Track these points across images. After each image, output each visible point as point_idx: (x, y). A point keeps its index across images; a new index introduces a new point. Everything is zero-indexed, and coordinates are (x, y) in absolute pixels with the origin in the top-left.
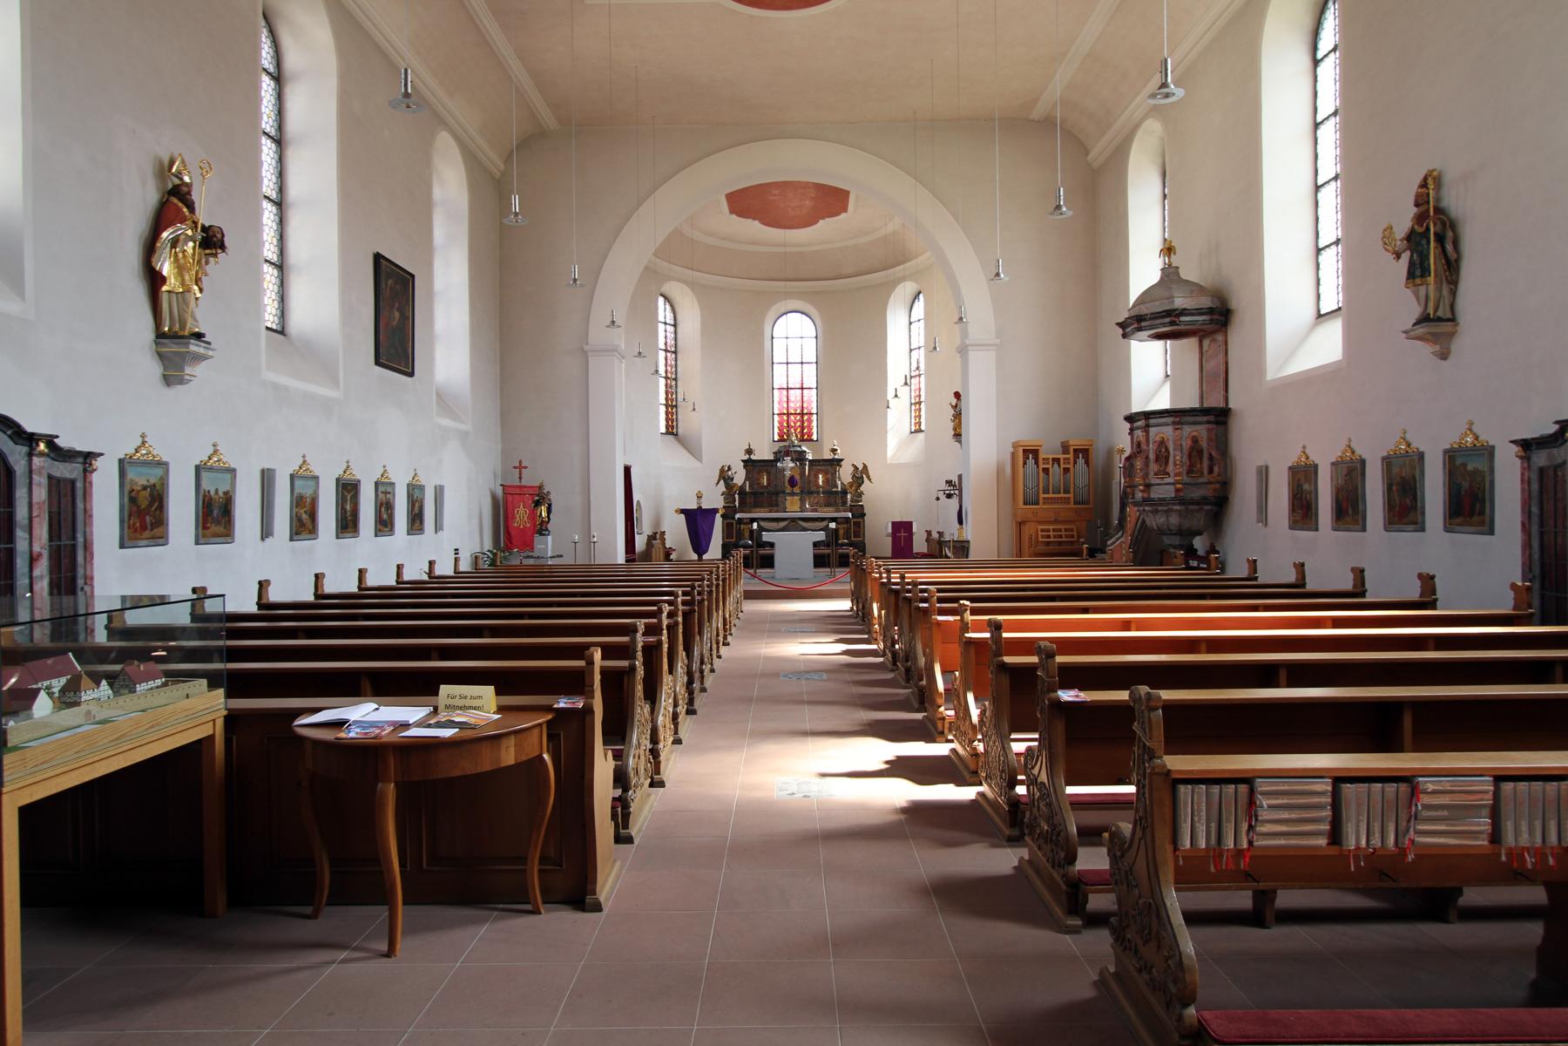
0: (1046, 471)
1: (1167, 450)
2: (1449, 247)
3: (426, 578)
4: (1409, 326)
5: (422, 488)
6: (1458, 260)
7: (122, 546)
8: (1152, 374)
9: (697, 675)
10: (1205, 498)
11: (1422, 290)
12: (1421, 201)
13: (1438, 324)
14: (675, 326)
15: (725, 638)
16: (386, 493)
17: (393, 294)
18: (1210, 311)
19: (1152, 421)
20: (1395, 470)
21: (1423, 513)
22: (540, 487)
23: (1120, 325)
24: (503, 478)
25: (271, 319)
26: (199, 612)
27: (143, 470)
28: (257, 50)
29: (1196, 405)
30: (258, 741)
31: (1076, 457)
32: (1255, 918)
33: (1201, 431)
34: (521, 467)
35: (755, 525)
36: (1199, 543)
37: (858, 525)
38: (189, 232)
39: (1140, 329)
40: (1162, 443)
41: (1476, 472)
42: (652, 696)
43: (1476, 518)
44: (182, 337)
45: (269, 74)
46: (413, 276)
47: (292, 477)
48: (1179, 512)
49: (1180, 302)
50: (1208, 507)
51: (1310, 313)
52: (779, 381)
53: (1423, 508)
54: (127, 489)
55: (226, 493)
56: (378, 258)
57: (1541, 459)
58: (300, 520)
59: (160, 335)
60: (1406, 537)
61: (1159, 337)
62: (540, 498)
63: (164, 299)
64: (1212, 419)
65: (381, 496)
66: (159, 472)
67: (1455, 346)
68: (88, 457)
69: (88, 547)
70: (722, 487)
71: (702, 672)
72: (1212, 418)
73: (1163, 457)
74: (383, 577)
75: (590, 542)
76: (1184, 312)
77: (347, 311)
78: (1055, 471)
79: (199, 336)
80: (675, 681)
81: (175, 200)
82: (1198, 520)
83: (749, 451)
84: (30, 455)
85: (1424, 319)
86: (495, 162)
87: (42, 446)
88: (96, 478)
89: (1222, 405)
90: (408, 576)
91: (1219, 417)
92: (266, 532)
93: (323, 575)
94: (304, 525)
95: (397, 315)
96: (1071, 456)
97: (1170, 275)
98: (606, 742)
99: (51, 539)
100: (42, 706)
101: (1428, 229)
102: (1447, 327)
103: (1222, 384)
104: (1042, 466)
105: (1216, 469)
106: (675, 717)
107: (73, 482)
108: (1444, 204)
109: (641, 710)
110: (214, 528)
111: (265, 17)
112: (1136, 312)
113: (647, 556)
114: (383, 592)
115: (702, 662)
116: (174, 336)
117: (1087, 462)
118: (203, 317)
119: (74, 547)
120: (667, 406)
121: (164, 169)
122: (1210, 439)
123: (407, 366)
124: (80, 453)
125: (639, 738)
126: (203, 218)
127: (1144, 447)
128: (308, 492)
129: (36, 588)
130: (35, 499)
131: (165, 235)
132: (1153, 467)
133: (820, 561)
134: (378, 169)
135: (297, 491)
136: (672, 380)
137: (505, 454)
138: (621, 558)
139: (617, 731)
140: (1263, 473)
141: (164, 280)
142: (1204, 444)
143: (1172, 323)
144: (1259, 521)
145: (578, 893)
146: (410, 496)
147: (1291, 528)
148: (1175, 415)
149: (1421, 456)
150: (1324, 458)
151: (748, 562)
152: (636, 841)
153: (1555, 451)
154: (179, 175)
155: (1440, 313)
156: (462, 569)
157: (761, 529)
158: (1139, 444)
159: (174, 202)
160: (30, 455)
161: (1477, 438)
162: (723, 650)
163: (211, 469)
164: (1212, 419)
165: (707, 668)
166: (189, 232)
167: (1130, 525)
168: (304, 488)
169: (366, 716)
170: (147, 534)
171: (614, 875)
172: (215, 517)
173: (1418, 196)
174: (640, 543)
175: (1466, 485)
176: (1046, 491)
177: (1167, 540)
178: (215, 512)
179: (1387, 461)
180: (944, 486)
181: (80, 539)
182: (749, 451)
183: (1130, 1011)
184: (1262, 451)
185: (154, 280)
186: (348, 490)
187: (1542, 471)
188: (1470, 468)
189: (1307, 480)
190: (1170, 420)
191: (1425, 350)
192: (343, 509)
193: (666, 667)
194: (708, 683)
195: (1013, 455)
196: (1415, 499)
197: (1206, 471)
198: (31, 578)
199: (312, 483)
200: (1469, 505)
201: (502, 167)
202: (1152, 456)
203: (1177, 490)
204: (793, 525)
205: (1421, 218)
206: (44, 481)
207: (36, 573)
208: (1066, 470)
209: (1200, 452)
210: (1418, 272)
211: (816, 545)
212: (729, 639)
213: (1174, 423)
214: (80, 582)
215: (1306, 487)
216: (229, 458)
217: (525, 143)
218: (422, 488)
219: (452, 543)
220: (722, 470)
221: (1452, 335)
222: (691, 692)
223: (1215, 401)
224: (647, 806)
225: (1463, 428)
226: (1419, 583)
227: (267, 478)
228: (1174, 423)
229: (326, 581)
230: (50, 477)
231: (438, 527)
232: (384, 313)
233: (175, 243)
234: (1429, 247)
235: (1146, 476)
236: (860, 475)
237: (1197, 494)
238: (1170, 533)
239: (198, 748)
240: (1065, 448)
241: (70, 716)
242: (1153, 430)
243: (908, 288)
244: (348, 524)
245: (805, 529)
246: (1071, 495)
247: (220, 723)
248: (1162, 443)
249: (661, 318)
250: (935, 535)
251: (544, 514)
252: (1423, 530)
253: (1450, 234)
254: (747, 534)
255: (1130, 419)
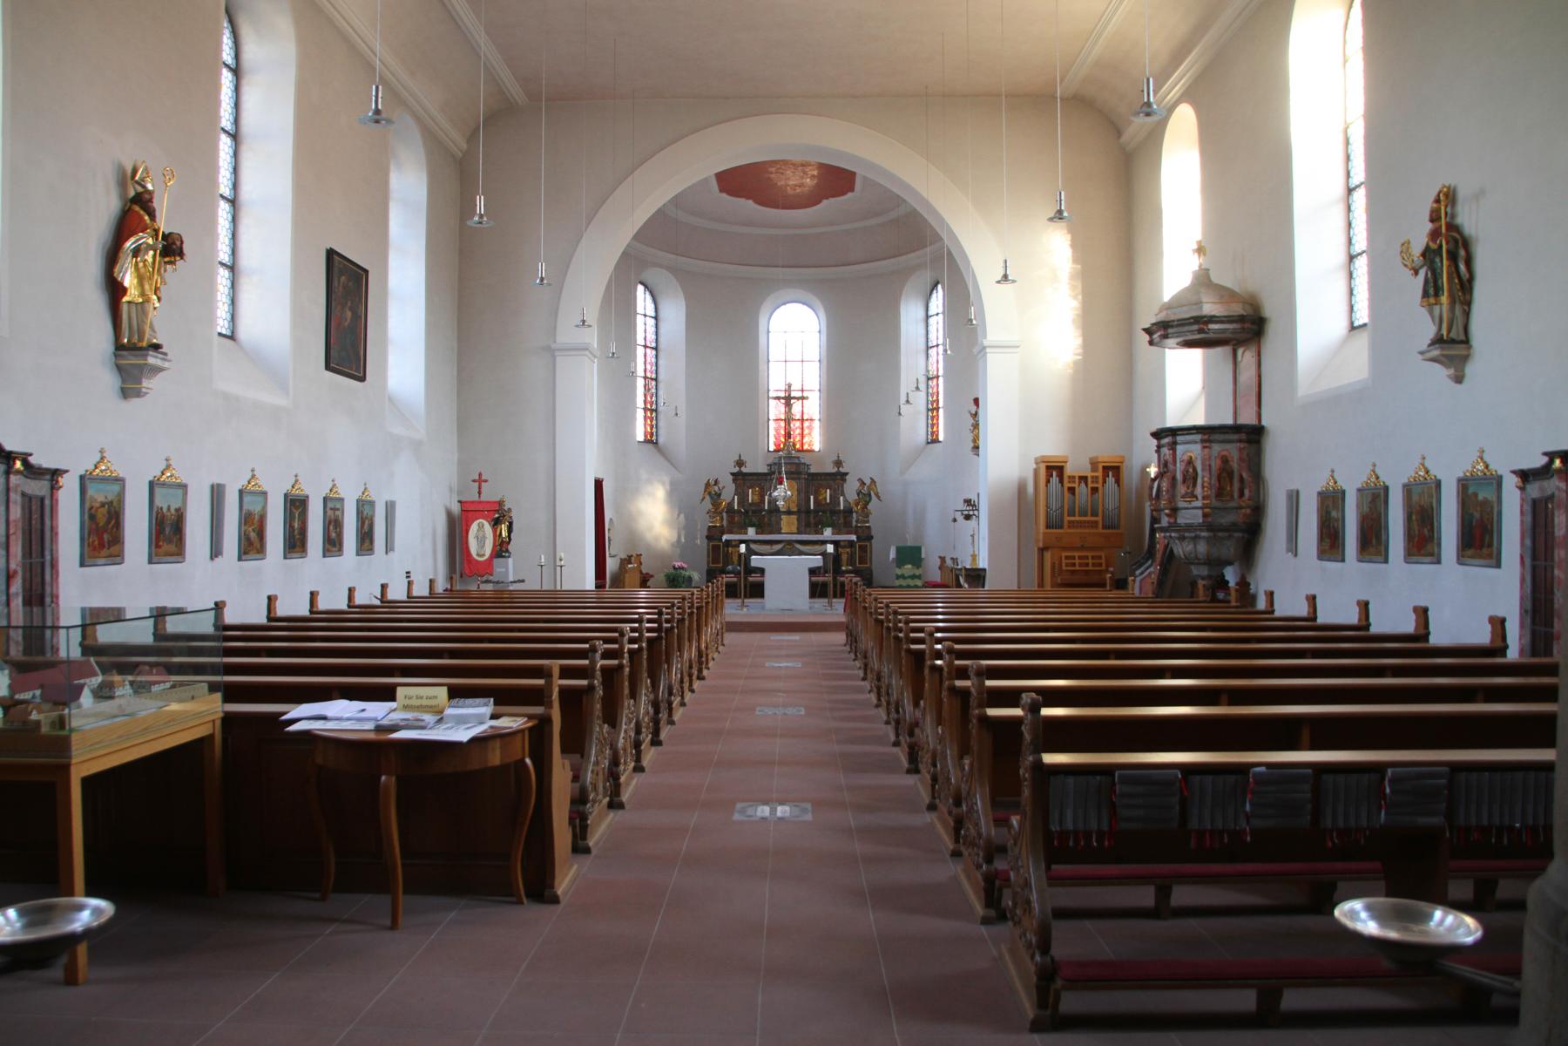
0: (1072, 490)
1: (1195, 470)
2: (1462, 267)
3: (378, 603)
4: (1424, 347)
5: (372, 504)
6: (1471, 279)
7: (82, 565)
8: (1186, 385)
9: (663, 706)
10: (1234, 524)
11: (1437, 309)
12: (1435, 217)
13: (1453, 347)
14: (656, 318)
15: (700, 671)
16: (334, 509)
17: (346, 289)
18: (1241, 319)
19: (1179, 438)
20: (1415, 498)
21: (1439, 545)
22: (501, 503)
23: (1147, 331)
24: (459, 493)
25: (223, 326)
26: (89, 642)
27: (101, 486)
28: (219, 50)
29: (1230, 421)
30: (252, 744)
31: (1105, 476)
32: (1160, 911)
33: (1233, 451)
34: (480, 481)
35: (743, 548)
36: (1231, 575)
37: (863, 549)
38: (150, 241)
39: (1166, 337)
40: (1190, 462)
41: (1486, 502)
42: (611, 719)
43: (1485, 551)
44: (141, 349)
45: (227, 66)
46: (366, 272)
47: (241, 492)
48: (1208, 539)
49: (1209, 309)
50: (1237, 535)
51: (1341, 326)
52: (776, 385)
53: (1439, 538)
54: (87, 505)
55: (177, 510)
56: (331, 254)
57: (1534, 490)
58: (248, 539)
59: (119, 347)
60: (1424, 569)
61: (1190, 344)
62: (499, 515)
63: (125, 308)
64: (1241, 442)
65: (330, 513)
66: (116, 488)
67: (1470, 369)
68: (55, 474)
69: (54, 565)
70: (708, 504)
71: (670, 704)
72: (1243, 436)
73: (1191, 478)
74: (332, 600)
75: (555, 565)
76: (1212, 319)
77: (298, 313)
78: (1082, 491)
79: (157, 347)
80: (637, 705)
81: (137, 208)
82: (1229, 549)
83: (740, 463)
84: (8, 473)
85: (1438, 341)
86: (458, 141)
87: (18, 464)
88: (62, 495)
89: (1254, 422)
90: (360, 600)
91: (1252, 436)
92: (216, 551)
93: (276, 597)
94: (252, 545)
95: (349, 314)
96: (1100, 474)
97: (1203, 280)
98: (565, 750)
99: (24, 556)
100: (86, 699)
101: (1440, 246)
102: (1458, 350)
103: (1254, 398)
104: (1067, 485)
105: (1247, 492)
106: (637, 745)
107: (42, 499)
108: (1459, 220)
109: (599, 729)
110: (166, 547)
111: (227, 11)
112: (1162, 317)
113: (618, 581)
114: (334, 616)
115: (670, 694)
116: (133, 348)
117: (1118, 481)
118: (162, 324)
119: (43, 565)
120: (645, 409)
121: (126, 178)
122: (1241, 459)
123: (358, 370)
124: (47, 471)
125: (597, 759)
126: (163, 225)
127: (1171, 466)
128: (257, 509)
129: (13, 604)
130: (12, 518)
131: (128, 244)
132: (1181, 489)
133: (817, 591)
134: (333, 165)
135: (245, 507)
136: (653, 380)
137: (463, 465)
138: (589, 583)
139: (575, 744)
140: (1294, 498)
141: (124, 291)
142: (1235, 465)
143: (1201, 331)
144: (1288, 550)
145: (541, 889)
146: (359, 512)
147: (1320, 558)
148: (1207, 433)
149: (1438, 484)
150: (1351, 484)
151: (732, 591)
152: (594, 852)
153: (1545, 483)
154: (141, 184)
155: (1453, 335)
156: (415, 593)
157: (750, 552)
158: (1166, 465)
159: (135, 210)
160: (8, 473)
161: (1487, 467)
162: (697, 684)
163: (164, 484)
164: (1241, 442)
165: (676, 701)
166: (150, 241)
167: (1159, 556)
168: (253, 505)
169: (343, 717)
170: (105, 552)
171: (568, 876)
172: (168, 535)
173: (1432, 212)
174: (611, 565)
175: (1477, 515)
176: (1072, 513)
177: (1195, 571)
178: (167, 530)
179: (1408, 489)
180: (961, 506)
181: (48, 557)
182: (740, 463)
183: (1013, 972)
184: (1293, 473)
185: (115, 290)
186: (296, 506)
187: (1535, 502)
188: (1480, 497)
189: (1336, 507)
190: (1198, 437)
191: (1441, 373)
192: (292, 527)
193: (626, 691)
194: (676, 717)
195: (1036, 472)
196: (1432, 530)
197: (1236, 495)
198: (8, 595)
199: (260, 499)
200: (1479, 539)
201: (465, 146)
202: (1179, 476)
203: (1205, 515)
204: (789, 548)
205: (1435, 234)
206: (19, 498)
207: (13, 590)
208: (1095, 490)
209: (1230, 474)
210: (1431, 291)
211: (813, 572)
212: (705, 672)
213: (1202, 441)
214: (48, 600)
215: (1334, 514)
216: (181, 474)
217: (492, 118)
218: (372, 504)
219: (408, 565)
220: (708, 485)
221: (1465, 358)
222: (656, 722)
223: (1247, 418)
224: (603, 826)
225: (1475, 456)
226: (1489, 627)
227: (217, 493)
228: (1202, 441)
229: (278, 603)
230: (23, 495)
231: (389, 547)
232: (336, 312)
233: (136, 252)
234: (1446, 264)
235: (1172, 499)
236: (865, 496)
237: (1226, 519)
238: (1196, 561)
239: (196, 748)
240: (1094, 464)
241: (106, 706)
242: (1179, 448)
243: (927, 277)
244: (295, 543)
245: (801, 553)
246: (1099, 519)
247: (218, 723)
248: (1190, 462)
249: (640, 309)
250: (949, 563)
251: (504, 534)
252: (1439, 562)
253: (1462, 253)
254: (735, 559)
255: (1158, 435)
